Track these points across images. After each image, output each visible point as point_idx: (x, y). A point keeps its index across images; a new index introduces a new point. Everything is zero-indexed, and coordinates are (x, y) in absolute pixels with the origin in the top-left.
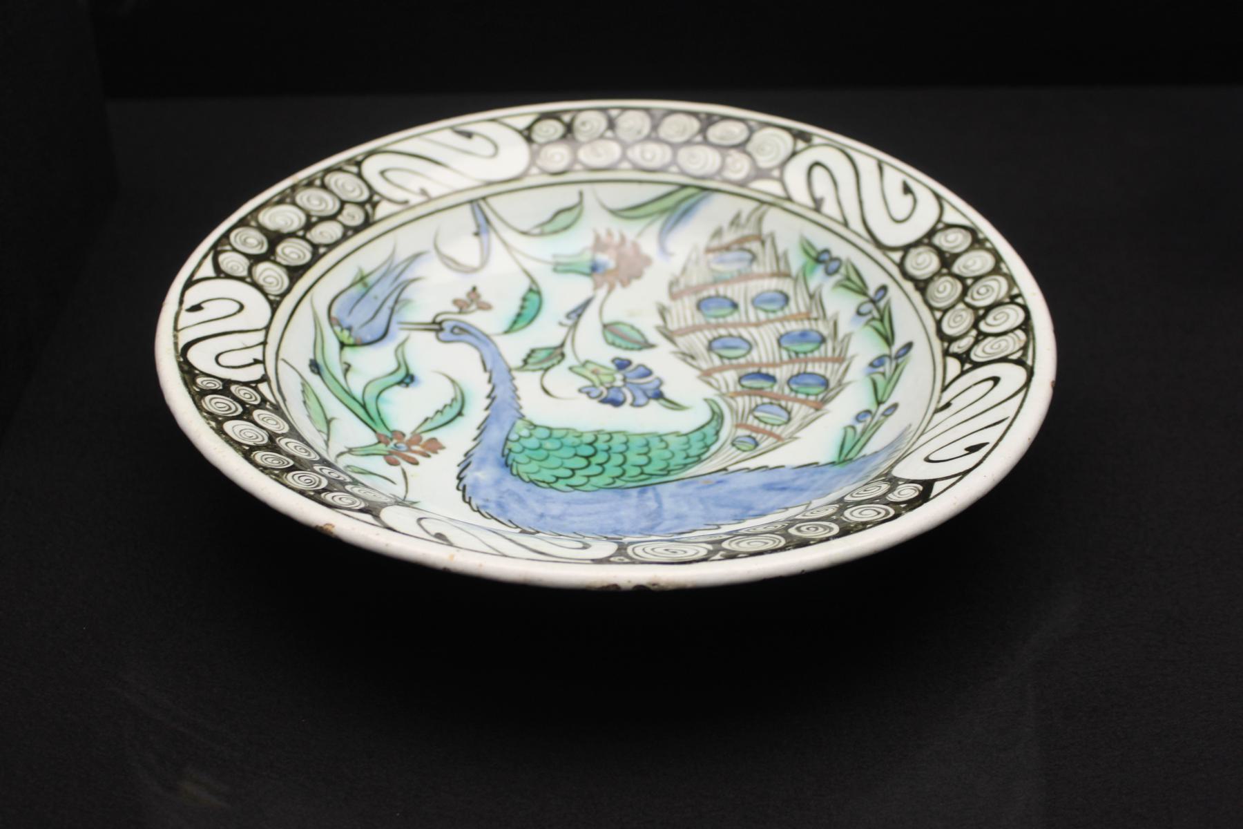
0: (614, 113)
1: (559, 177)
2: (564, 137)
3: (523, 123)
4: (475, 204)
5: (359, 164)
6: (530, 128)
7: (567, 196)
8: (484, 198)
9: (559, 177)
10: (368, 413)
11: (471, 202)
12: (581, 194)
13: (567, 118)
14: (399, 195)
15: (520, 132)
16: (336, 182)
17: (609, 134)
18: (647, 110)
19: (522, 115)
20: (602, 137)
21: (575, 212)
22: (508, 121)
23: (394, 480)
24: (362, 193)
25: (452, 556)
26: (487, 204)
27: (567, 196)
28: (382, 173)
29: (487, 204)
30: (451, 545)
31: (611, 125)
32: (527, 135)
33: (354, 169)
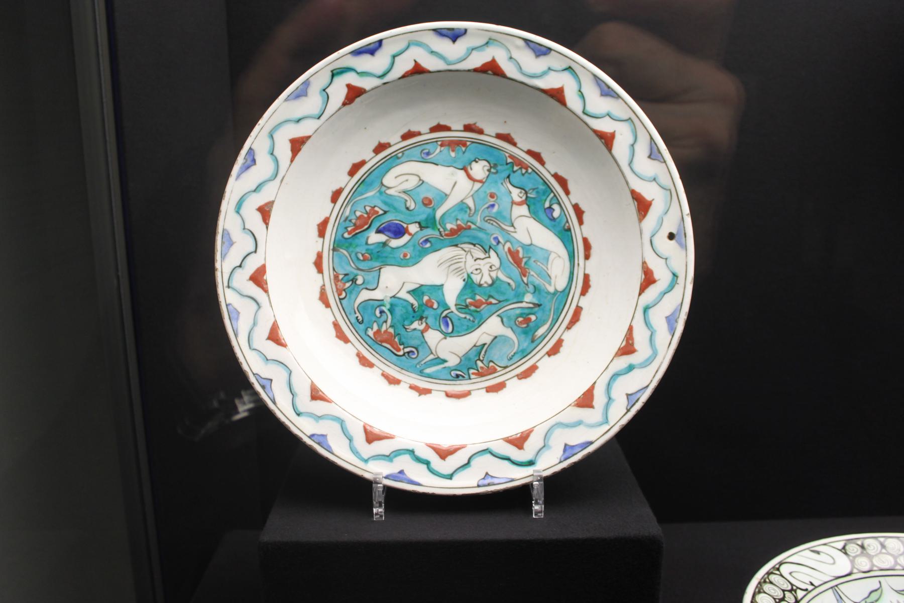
0: (882, 540)
1: (867, 574)
2: (862, 553)
3: (840, 545)
4: (833, 588)
5: (778, 569)
6: (844, 548)
7: (873, 584)
8: (836, 586)
9: (867, 574)
10: (473, 322)
11: (832, 588)
12: (880, 582)
13: (859, 542)
14: (804, 586)
15: (840, 550)
16: (774, 578)
17: (884, 551)
18: (898, 538)
19: (838, 541)
20: (881, 553)
21: (879, 591)
22: (832, 544)
23: (451, 354)
24: (788, 587)
25: (688, 215)
26: (838, 588)
27: (873, 584)
28: (790, 573)
29: (838, 588)
30: (640, 294)
31: (883, 546)
32: (844, 550)
33: (777, 572)
